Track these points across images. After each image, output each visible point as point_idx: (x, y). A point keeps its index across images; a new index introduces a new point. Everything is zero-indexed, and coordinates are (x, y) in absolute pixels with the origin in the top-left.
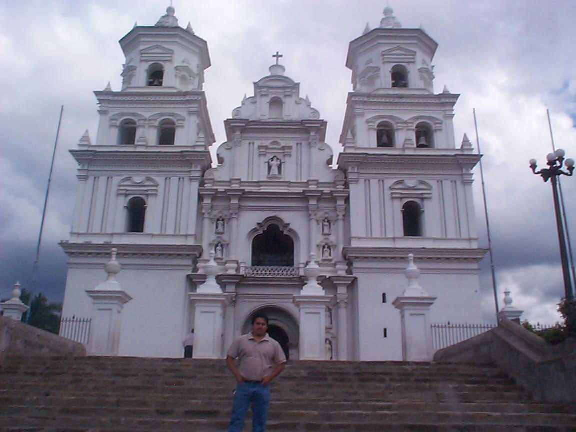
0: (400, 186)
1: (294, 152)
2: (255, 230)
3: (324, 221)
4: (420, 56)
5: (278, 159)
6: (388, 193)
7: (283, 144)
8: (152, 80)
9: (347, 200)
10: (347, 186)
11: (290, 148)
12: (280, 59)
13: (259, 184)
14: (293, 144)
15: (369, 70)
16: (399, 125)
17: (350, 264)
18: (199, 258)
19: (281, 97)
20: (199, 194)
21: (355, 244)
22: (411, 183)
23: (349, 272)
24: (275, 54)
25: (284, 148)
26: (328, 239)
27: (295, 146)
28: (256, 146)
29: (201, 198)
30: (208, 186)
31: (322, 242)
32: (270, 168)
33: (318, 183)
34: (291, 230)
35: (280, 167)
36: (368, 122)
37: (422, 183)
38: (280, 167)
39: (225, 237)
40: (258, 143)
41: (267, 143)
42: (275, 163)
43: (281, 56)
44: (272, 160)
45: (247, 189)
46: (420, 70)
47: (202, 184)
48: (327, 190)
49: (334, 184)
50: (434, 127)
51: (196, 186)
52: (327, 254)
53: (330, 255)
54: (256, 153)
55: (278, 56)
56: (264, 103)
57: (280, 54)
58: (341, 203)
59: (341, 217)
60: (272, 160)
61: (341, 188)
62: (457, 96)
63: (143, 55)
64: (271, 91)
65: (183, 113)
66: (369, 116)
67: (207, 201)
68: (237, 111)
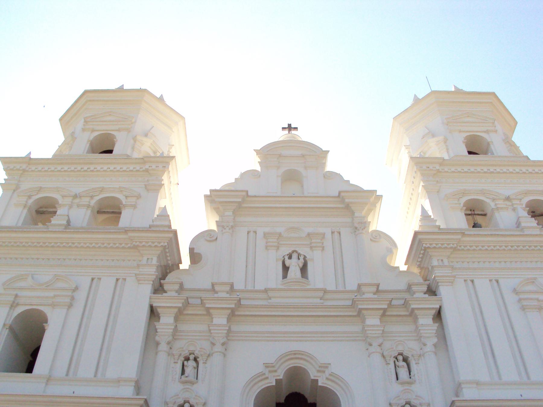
2: (260, 376)
24: (287, 126)
28: (260, 232)
32: (286, 269)
38: (304, 269)
44: (290, 257)
55: (290, 128)
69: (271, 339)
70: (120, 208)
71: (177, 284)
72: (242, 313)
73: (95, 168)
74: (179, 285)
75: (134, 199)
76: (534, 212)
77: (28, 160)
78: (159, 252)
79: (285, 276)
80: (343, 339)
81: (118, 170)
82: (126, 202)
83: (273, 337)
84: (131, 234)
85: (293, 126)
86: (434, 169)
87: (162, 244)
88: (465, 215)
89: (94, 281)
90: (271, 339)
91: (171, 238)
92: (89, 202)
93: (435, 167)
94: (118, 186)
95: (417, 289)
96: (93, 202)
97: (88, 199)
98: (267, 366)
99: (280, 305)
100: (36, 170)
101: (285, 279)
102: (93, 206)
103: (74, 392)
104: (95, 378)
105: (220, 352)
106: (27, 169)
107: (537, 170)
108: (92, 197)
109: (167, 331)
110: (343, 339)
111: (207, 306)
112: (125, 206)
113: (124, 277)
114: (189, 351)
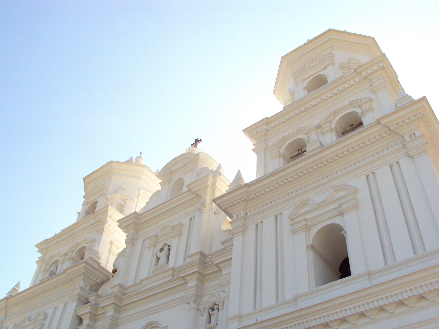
69: (165, 308)
70: (360, 118)
71: (198, 253)
72: (125, 304)
73: (321, 100)
74: (199, 254)
75: (368, 104)
76: (352, 125)
77: (267, 121)
78: (82, 278)
79: (157, 263)
80: (178, 303)
81: (336, 93)
82: (307, 137)
83: (166, 306)
84: (67, 272)
86: (263, 130)
87: (82, 272)
88: (306, 150)
89: (277, 218)
90: (165, 308)
91: (85, 266)
92: (279, 151)
93: (339, 90)
94: (348, 103)
95: (227, 245)
96: (333, 126)
97: (327, 125)
99: (177, 277)
100: (296, 114)
101: (157, 266)
102: (335, 127)
103: (257, 320)
104: (386, 266)
105: (193, 308)
106: (268, 128)
107: (319, 101)
108: (330, 122)
109: (190, 293)
110: (178, 303)
111: (215, 263)
112: (363, 113)
113: (261, 221)
114: (212, 302)
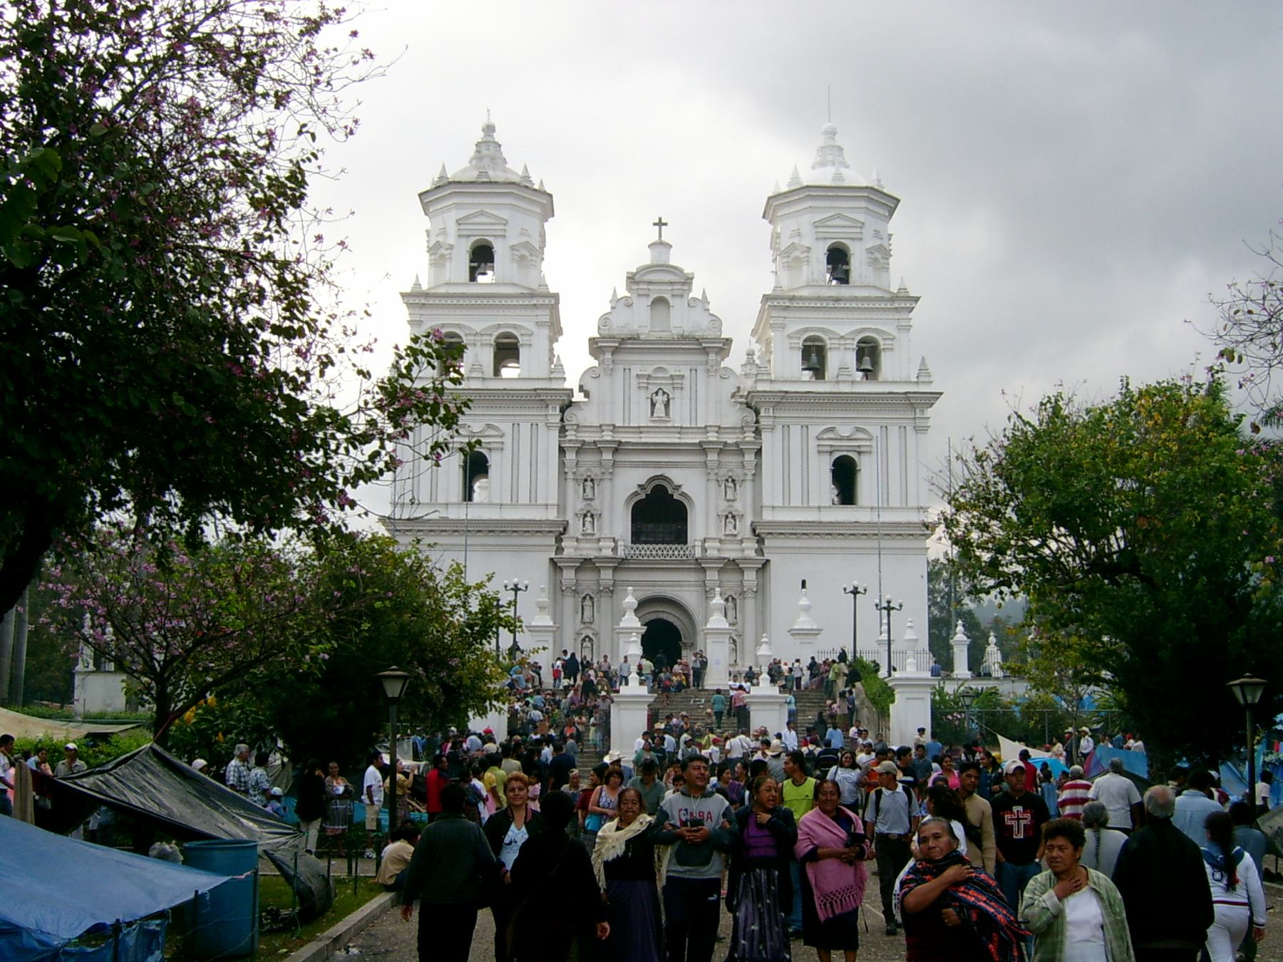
0: (831, 435)
1: (686, 383)
2: (636, 494)
3: (727, 480)
4: (871, 224)
5: (664, 393)
6: (813, 444)
7: (672, 371)
8: (475, 264)
9: (759, 452)
10: (758, 432)
11: (682, 377)
12: (663, 227)
13: (639, 430)
14: (685, 371)
15: (793, 247)
16: (833, 341)
17: (760, 541)
18: (563, 534)
19: (668, 296)
20: (560, 447)
21: (767, 516)
22: (845, 431)
23: (760, 551)
25: (672, 377)
26: (730, 506)
27: (687, 374)
29: (562, 451)
30: (571, 435)
31: (724, 510)
32: (653, 405)
33: (719, 429)
34: (683, 494)
35: (667, 405)
36: (789, 337)
37: (858, 430)
38: (667, 405)
39: (595, 504)
40: (636, 370)
41: (649, 370)
42: (660, 399)
43: (666, 224)
44: (657, 393)
45: (624, 438)
46: (870, 251)
47: (563, 430)
48: (731, 439)
49: (742, 429)
50: (882, 344)
51: (555, 434)
52: (730, 526)
53: (735, 528)
54: (634, 383)
56: (642, 305)
57: (663, 221)
58: (749, 457)
59: (749, 477)
60: (657, 393)
61: (750, 436)
62: (917, 299)
63: (462, 227)
64: (651, 287)
65: (530, 325)
66: (793, 328)
67: (570, 456)
68: (604, 320)
85: (663, 221)
98: (639, 486)
